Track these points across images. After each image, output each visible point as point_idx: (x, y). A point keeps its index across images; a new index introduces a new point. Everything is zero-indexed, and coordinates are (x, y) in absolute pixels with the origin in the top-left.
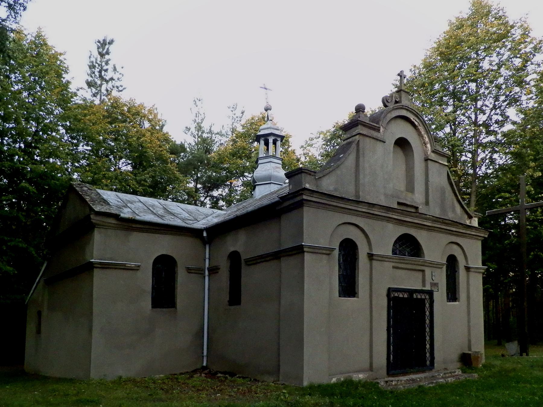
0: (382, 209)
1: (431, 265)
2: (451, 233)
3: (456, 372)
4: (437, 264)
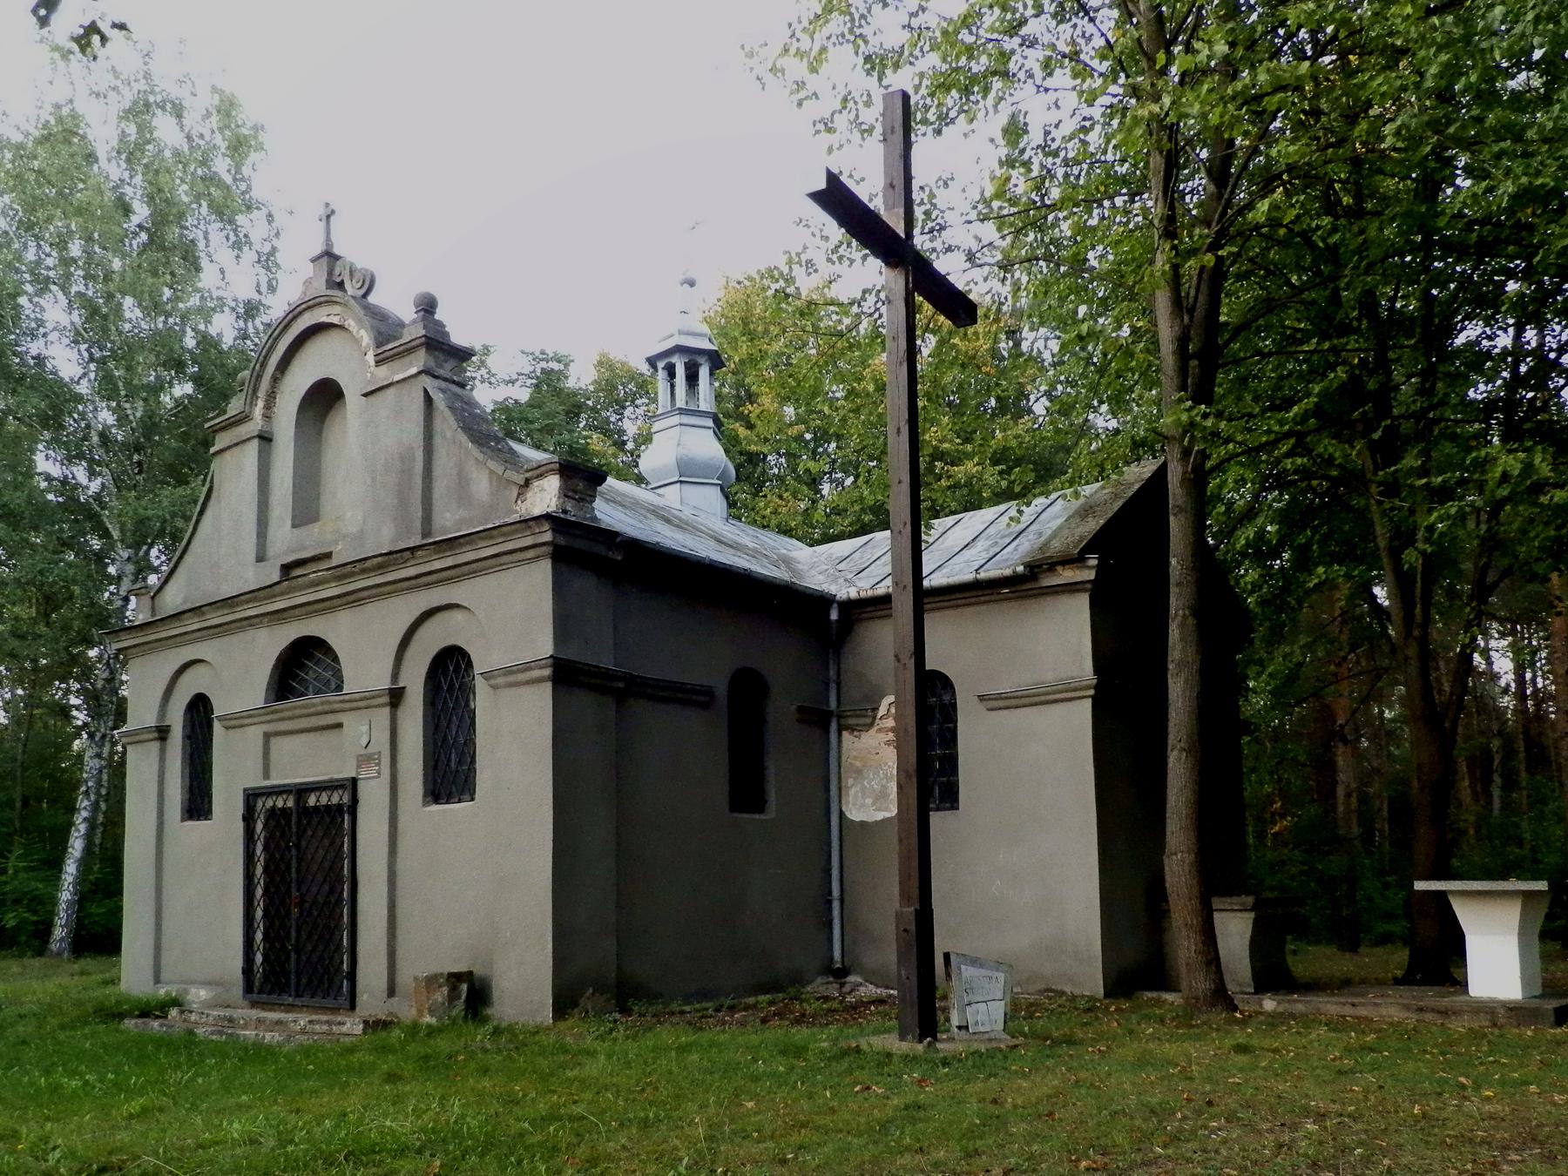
0: (222, 607)
1: (347, 705)
2: (278, 616)
3: (344, 1024)
4: (361, 700)
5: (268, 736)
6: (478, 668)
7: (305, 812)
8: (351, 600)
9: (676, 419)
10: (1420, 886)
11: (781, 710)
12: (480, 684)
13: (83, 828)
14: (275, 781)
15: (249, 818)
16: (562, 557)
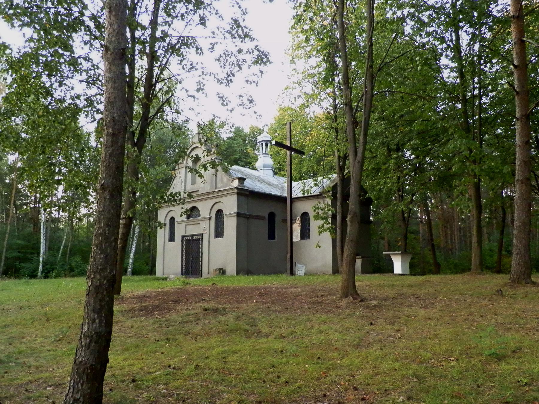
5: (186, 225)
6: (224, 214)
7: (193, 240)
8: (202, 200)
9: (263, 155)
10: (384, 253)
11: (278, 219)
12: (225, 216)
13: (135, 245)
14: (187, 234)
15: (182, 241)
16: (238, 194)
